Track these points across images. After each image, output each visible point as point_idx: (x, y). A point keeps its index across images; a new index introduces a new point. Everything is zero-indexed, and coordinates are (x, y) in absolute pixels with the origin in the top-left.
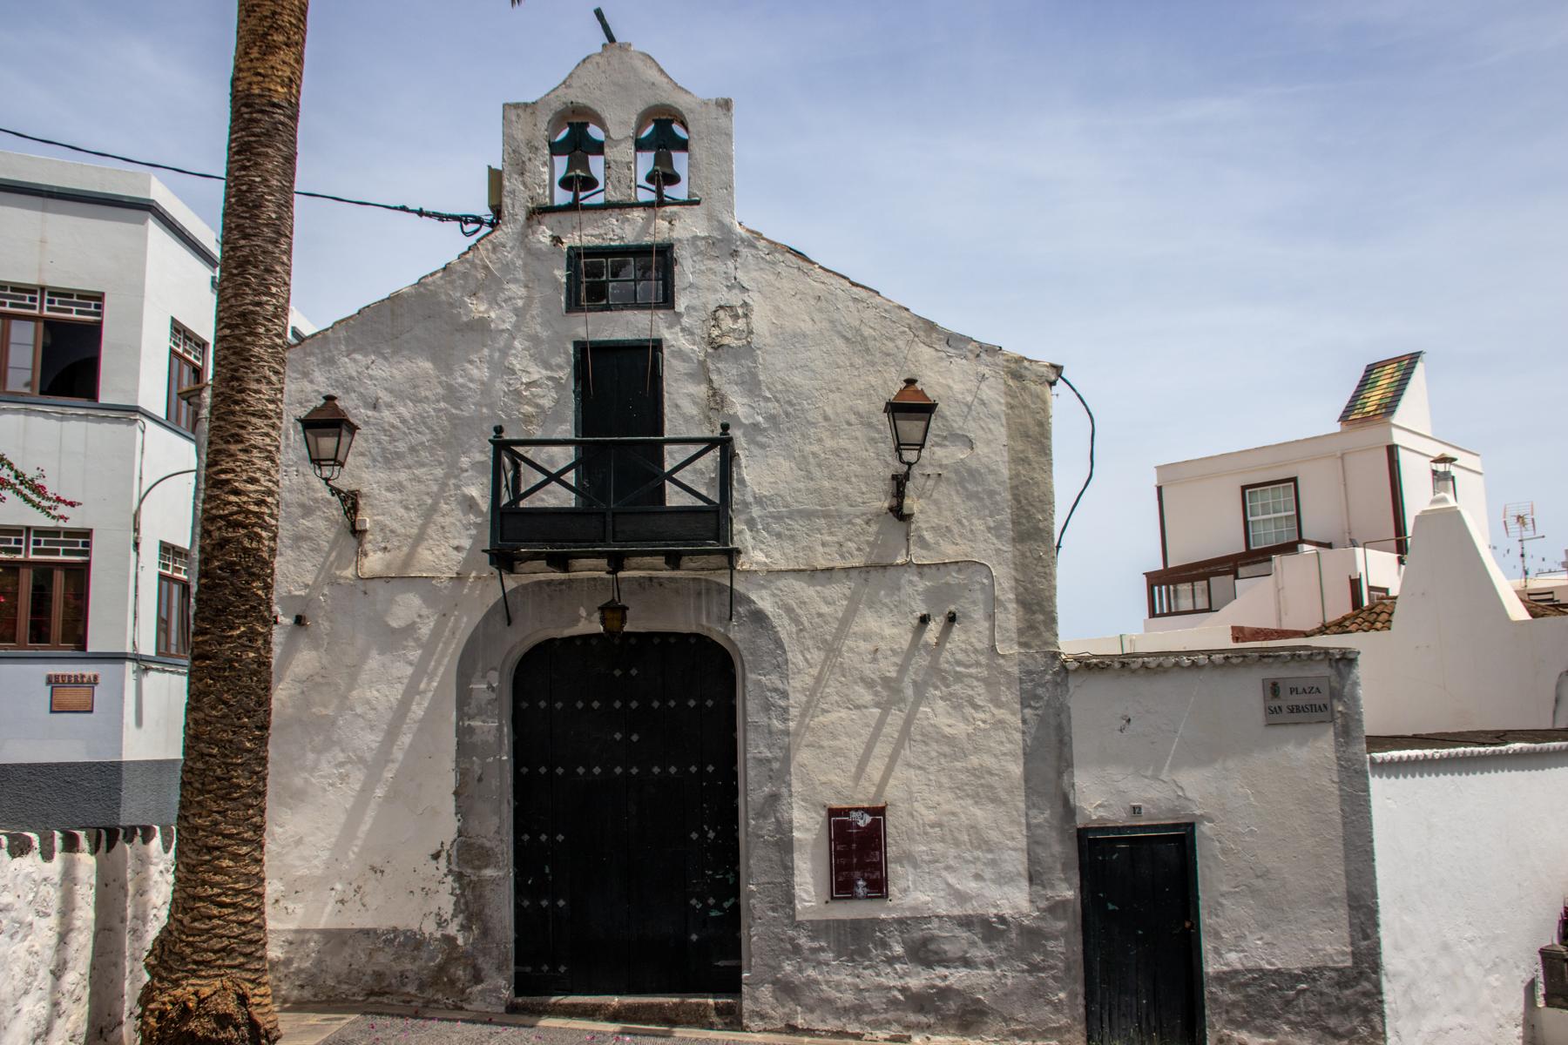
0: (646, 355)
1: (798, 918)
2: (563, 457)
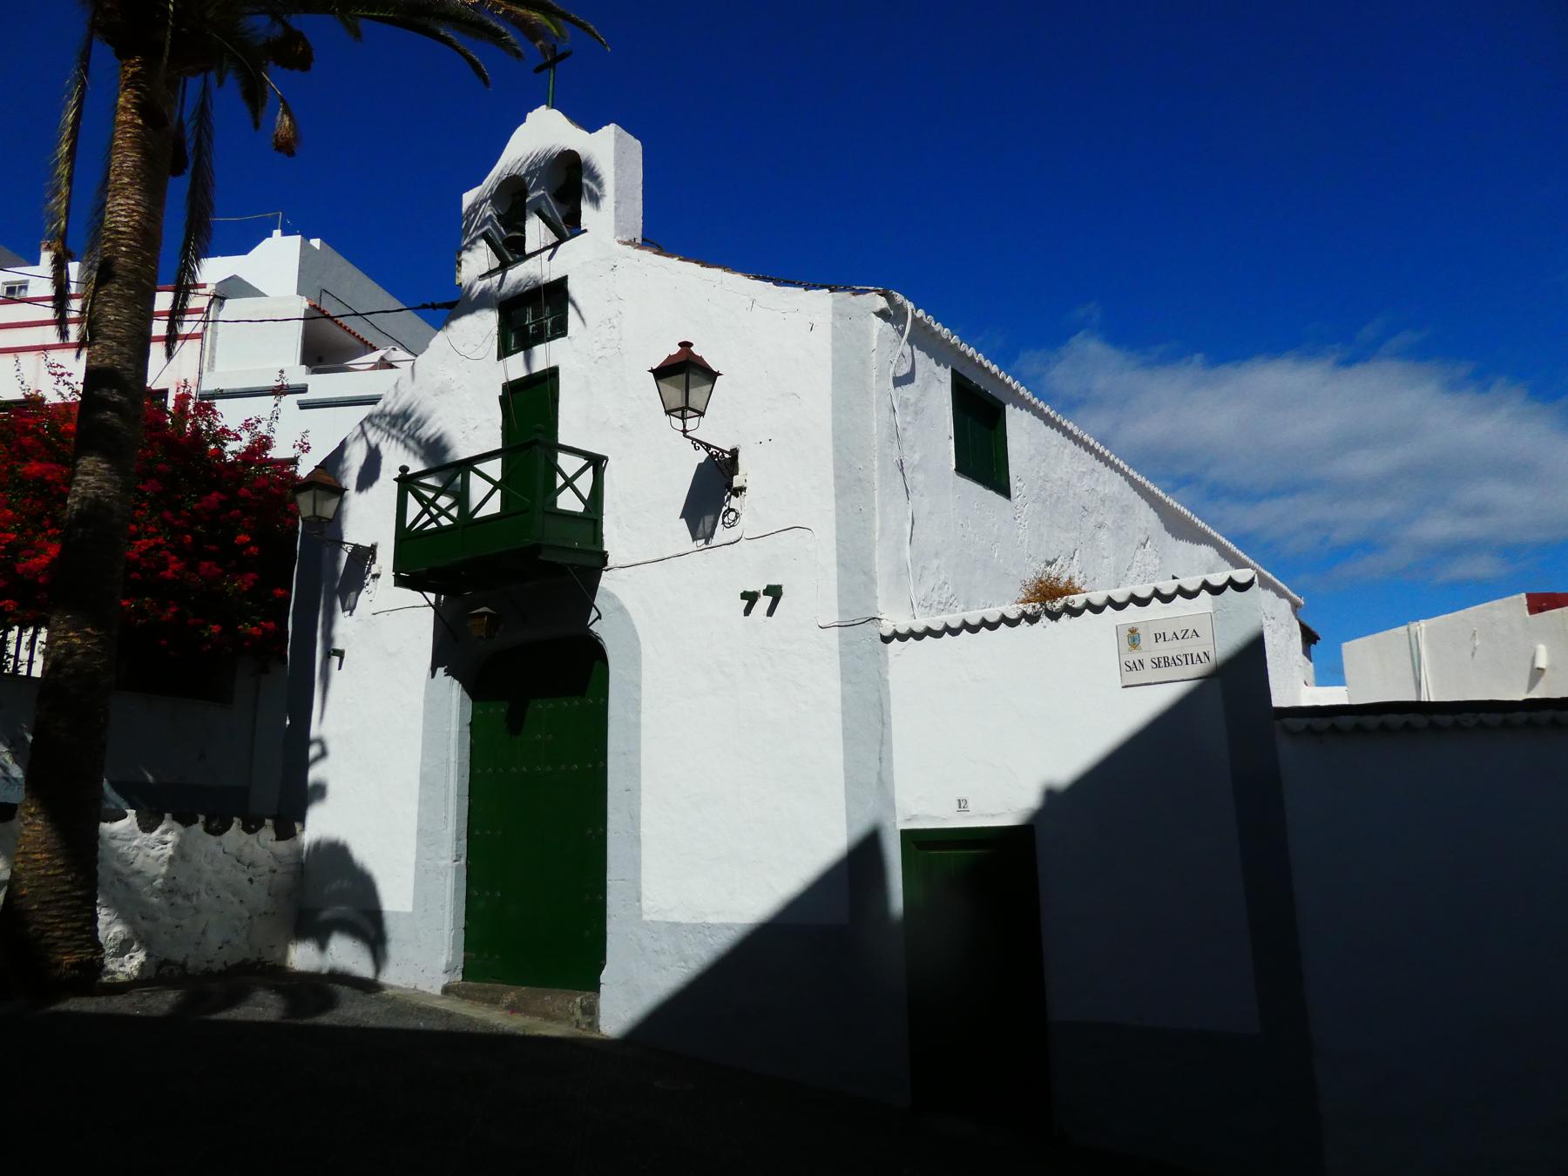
1: (646, 917)
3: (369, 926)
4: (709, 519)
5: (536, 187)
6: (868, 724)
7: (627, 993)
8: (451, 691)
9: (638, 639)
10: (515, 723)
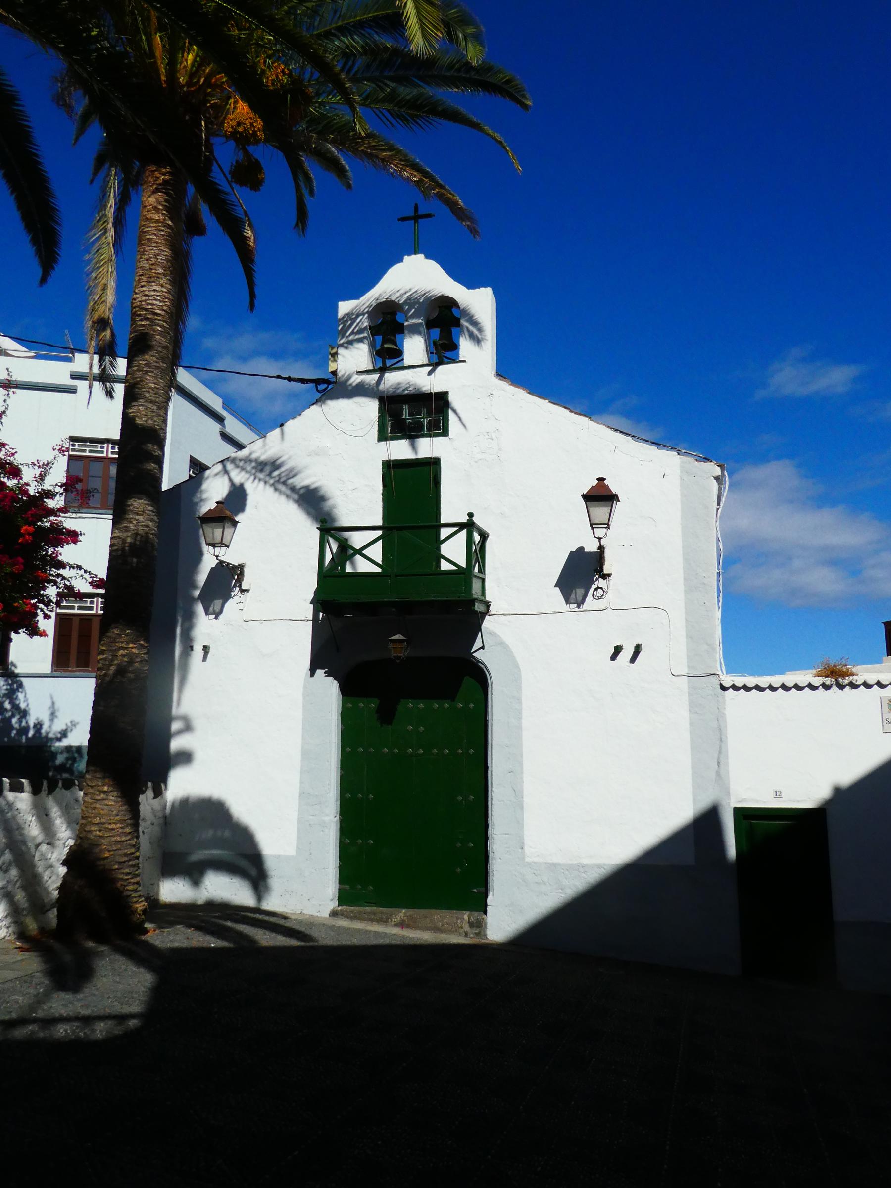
0: (431, 468)
1: (527, 860)
3: (250, 864)
4: (580, 592)
6: (710, 743)
7: (507, 915)
8: (328, 689)
9: (517, 667)
10: (386, 715)
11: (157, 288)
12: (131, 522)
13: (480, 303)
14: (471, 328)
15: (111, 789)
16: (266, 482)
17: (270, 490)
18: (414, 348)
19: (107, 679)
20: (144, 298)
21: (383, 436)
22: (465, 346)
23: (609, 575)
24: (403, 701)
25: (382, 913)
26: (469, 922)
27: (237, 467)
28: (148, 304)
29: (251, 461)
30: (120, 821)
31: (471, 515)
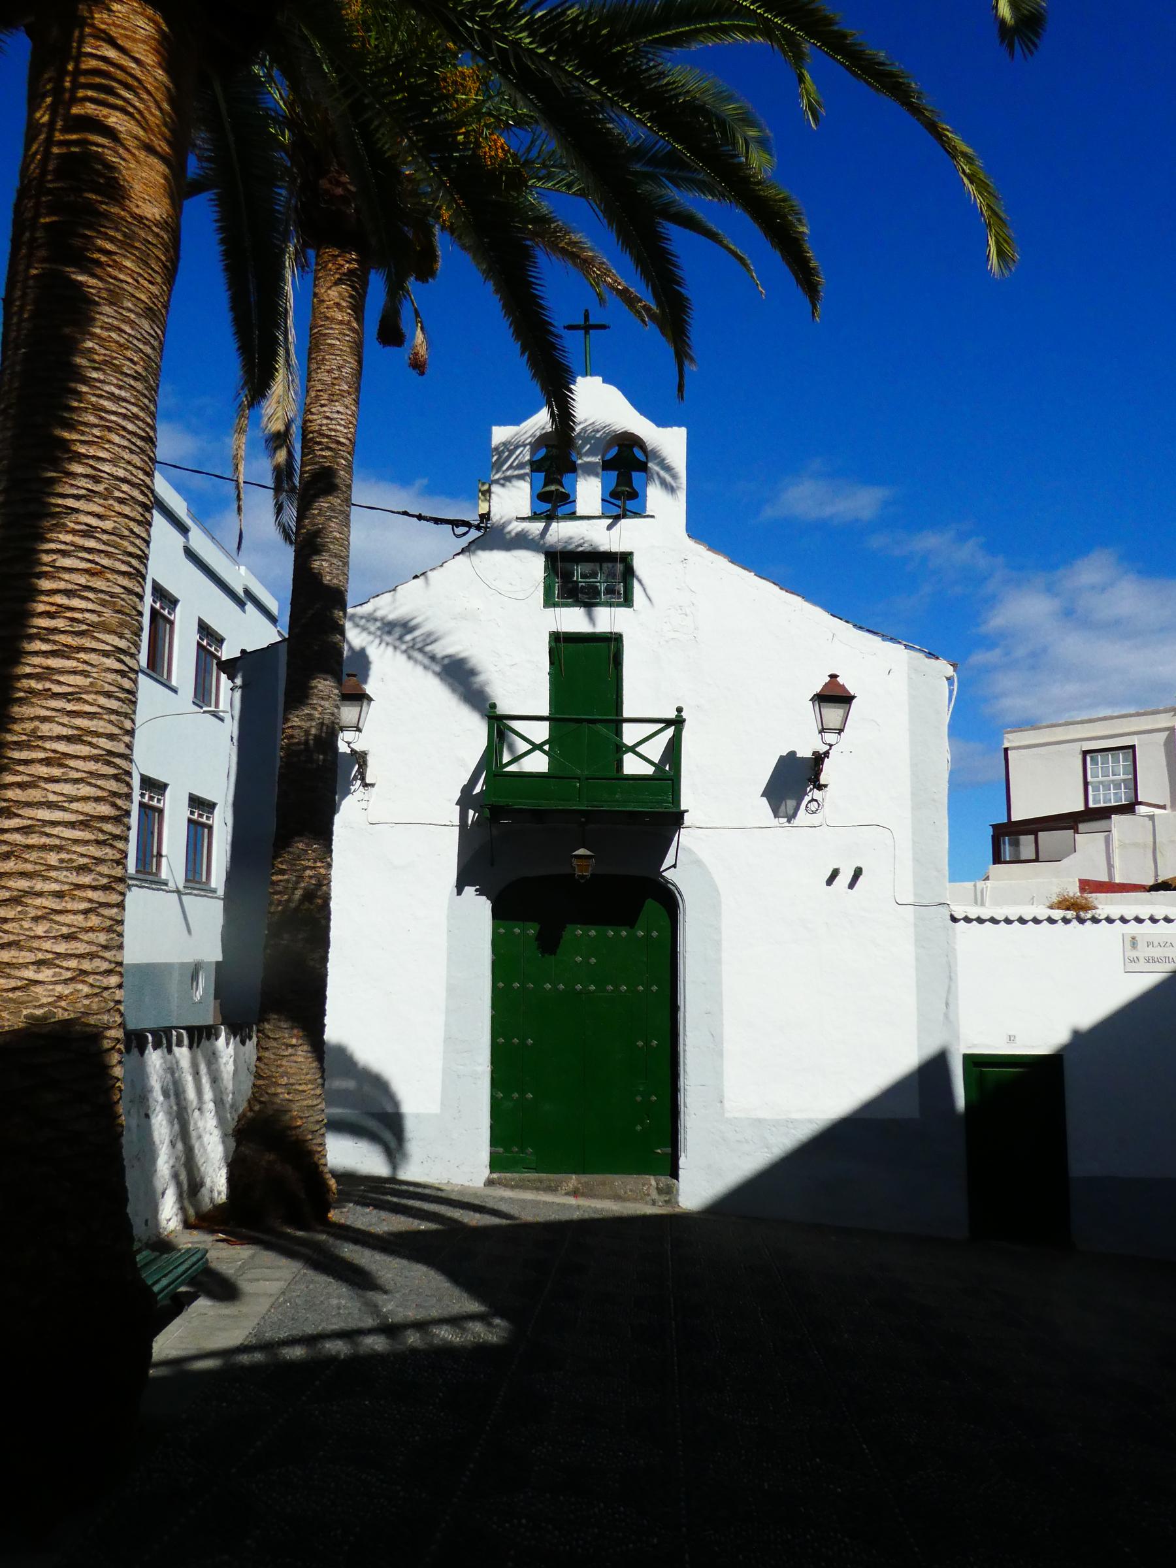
1: (727, 1115)
2: (540, 732)
4: (791, 803)
5: (590, 453)
6: (939, 982)
10: (549, 943)
11: (341, 409)
12: (315, 709)
13: (670, 443)
14: (662, 473)
15: (300, 1042)
16: (395, 648)
17: (401, 659)
18: (589, 492)
19: (292, 905)
20: (325, 421)
21: (549, 602)
22: (654, 495)
23: (825, 786)
24: (569, 927)
25: (550, 1180)
26: (657, 1188)
27: (357, 626)
28: (331, 430)
29: (376, 620)
30: (310, 1082)
31: (679, 710)
